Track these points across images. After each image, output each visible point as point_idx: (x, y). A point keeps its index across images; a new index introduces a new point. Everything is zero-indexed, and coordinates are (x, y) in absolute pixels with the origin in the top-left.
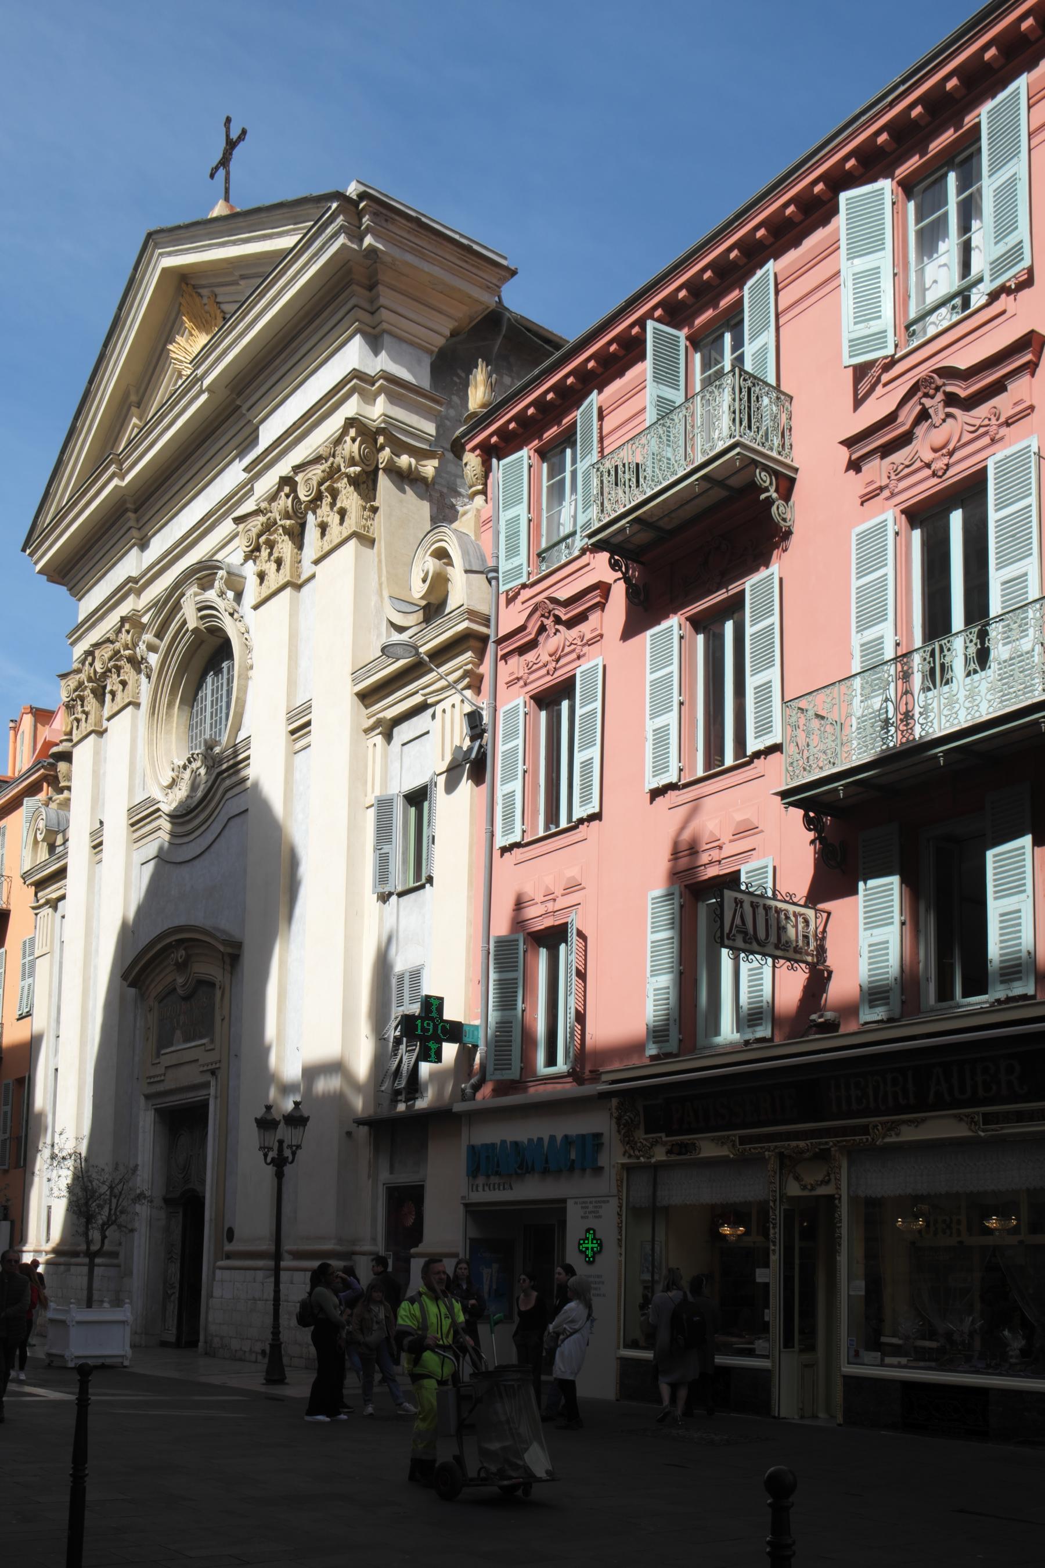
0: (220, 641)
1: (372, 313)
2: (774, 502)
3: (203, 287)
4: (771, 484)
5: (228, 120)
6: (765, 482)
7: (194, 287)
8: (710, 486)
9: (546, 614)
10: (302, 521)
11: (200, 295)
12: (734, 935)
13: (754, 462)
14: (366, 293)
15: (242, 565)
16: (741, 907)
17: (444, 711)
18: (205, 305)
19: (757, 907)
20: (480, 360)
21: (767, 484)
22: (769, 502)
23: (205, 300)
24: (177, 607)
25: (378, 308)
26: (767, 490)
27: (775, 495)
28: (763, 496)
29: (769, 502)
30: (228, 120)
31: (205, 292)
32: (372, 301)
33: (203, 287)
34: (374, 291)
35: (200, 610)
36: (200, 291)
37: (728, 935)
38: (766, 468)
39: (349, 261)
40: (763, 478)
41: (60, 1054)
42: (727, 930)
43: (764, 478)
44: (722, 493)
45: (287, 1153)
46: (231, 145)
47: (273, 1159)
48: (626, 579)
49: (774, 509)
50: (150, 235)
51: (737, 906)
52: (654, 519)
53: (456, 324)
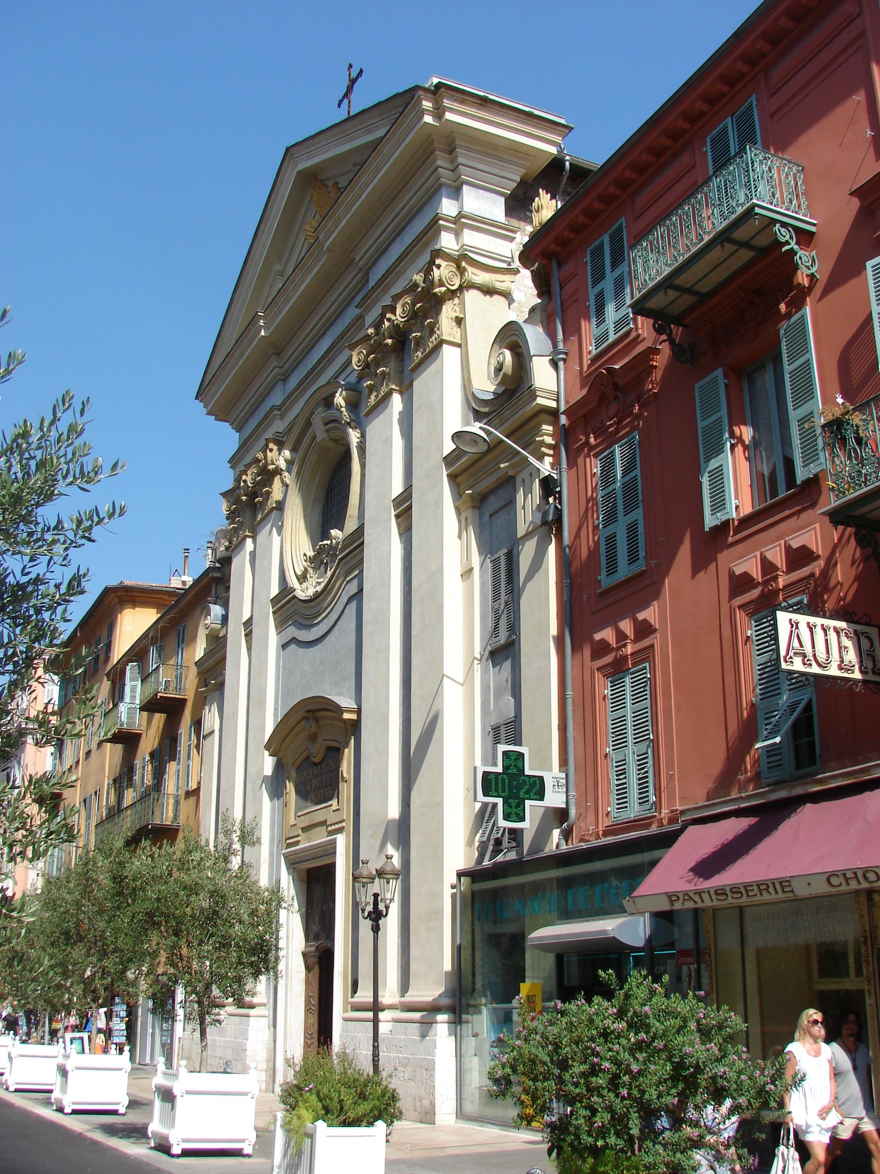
0: (346, 447)
1: (453, 171)
2: (796, 254)
3: (328, 179)
4: (791, 238)
5: (351, 66)
6: (784, 237)
7: (322, 181)
8: (736, 248)
9: (606, 384)
10: (403, 339)
11: (327, 187)
12: (791, 658)
13: (774, 221)
14: (448, 156)
15: (358, 382)
16: (797, 628)
17: (523, 480)
18: (330, 192)
19: (815, 626)
20: (540, 190)
21: (788, 237)
22: (792, 252)
23: (330, 189)
24: (308, 424)
25: (458, 166)
26: (787, 243)
27: (796, 247)
28: (784, 249)
29: (792, 252)
30: (351, 66)
31: (330, 183)
32: (452, 161)
33: (328, 179)
34: (454, 154)
35: (326, 424)
36: (325, 183)
37: (785, 657)
38: (784, 225)
39: (431, 135)
40: (784, 235)
41: (729, 608)
42: (783, 652)
43: (784, 234)
44: (749, 255)
45: (381, 907)
46: (353, 82)
47: (370, 913)
48: (671, 340)
49: (797, 257)
50: (288, 149)
51: (792, 627)
52: (690, 285)
53: (523, 171)
